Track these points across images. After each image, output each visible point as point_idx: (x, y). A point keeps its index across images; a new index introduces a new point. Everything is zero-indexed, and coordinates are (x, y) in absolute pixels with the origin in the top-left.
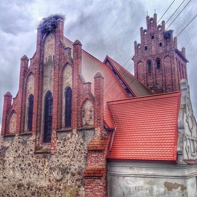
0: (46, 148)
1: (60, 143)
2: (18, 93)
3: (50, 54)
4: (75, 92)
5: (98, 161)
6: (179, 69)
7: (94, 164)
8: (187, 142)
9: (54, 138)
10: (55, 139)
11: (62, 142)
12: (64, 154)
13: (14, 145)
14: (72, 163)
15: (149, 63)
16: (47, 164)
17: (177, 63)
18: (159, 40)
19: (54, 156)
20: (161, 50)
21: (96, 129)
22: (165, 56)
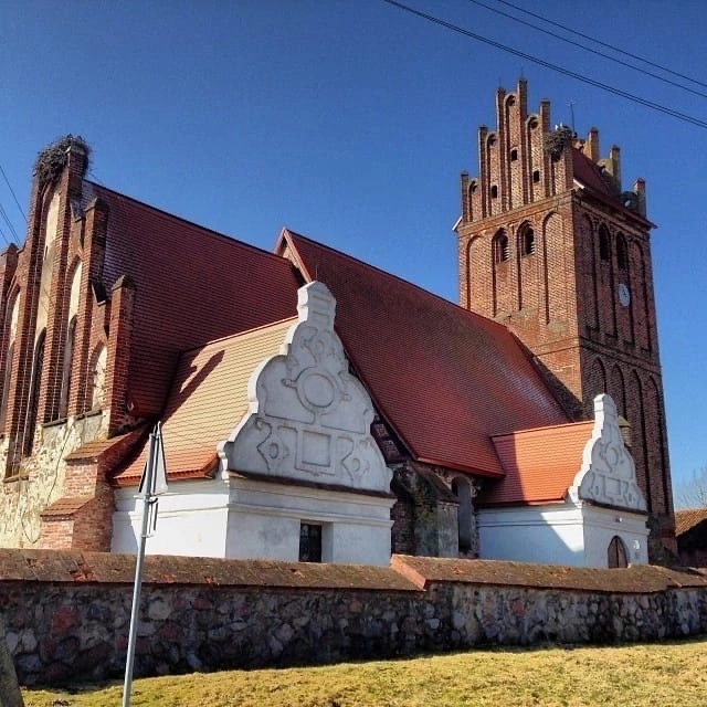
15: (500, 238)
22: (547, 212)
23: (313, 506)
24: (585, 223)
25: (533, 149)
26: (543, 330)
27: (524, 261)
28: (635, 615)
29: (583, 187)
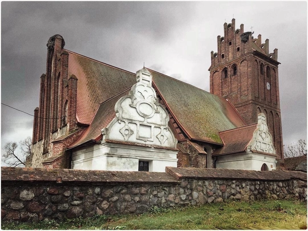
15: (225, 70)
18: (237, 45)
20: (238, 54)
22: (242, 60)
23: (145, 155)
24: (256, 63)
26: (239, 99)
28: (276, 190)
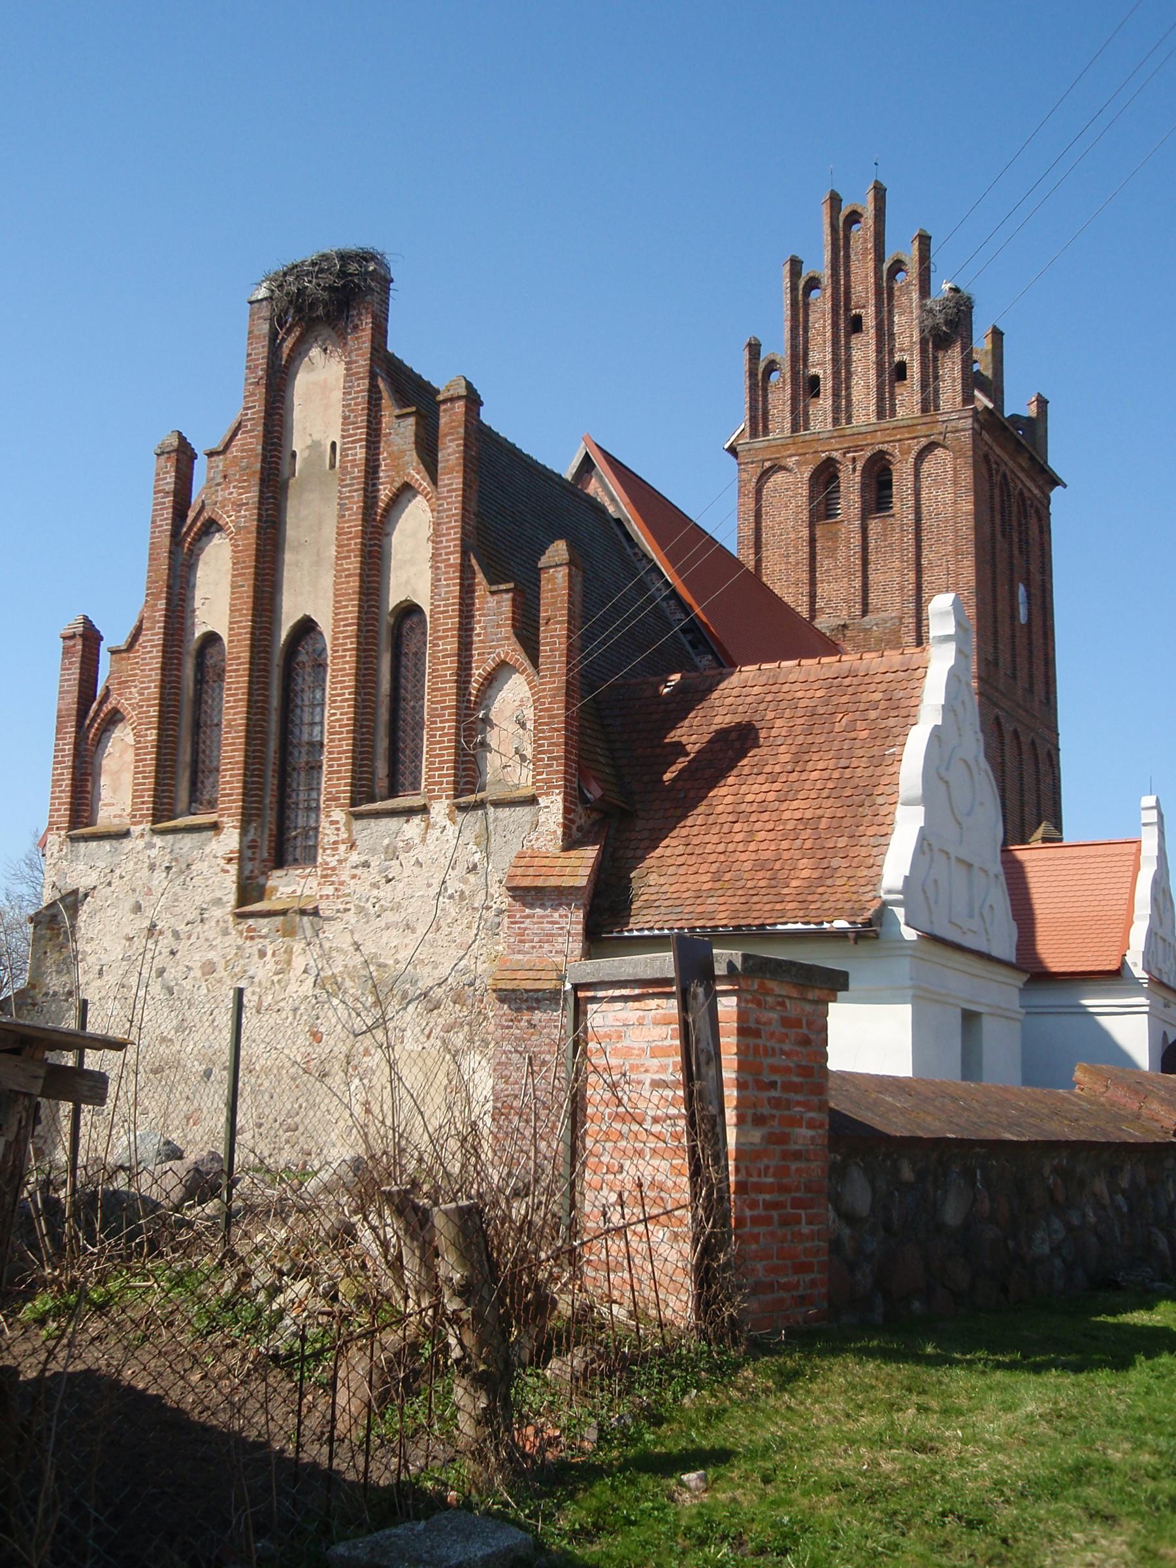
0: (294, 892)
1: (366, 865)
2: (141, 622)
3: (316, 437)
4: (444, 630)
5: (552, 935)
6: (998, 529)
7: (534, 947)
8: (932, 860)
9: (335, 843)
10: (342, 847)
11: (374, 862)
12: (390, 917)
13: (122, 877)
14: (424, 953)
15: (825, 477)
16: (299, 962)
17: (992, 490)
19: (338, 926)
21: (543, 801)
22: (924, 442)
25: (896, 319)
27: (874, 526)
29: (991, 406)
